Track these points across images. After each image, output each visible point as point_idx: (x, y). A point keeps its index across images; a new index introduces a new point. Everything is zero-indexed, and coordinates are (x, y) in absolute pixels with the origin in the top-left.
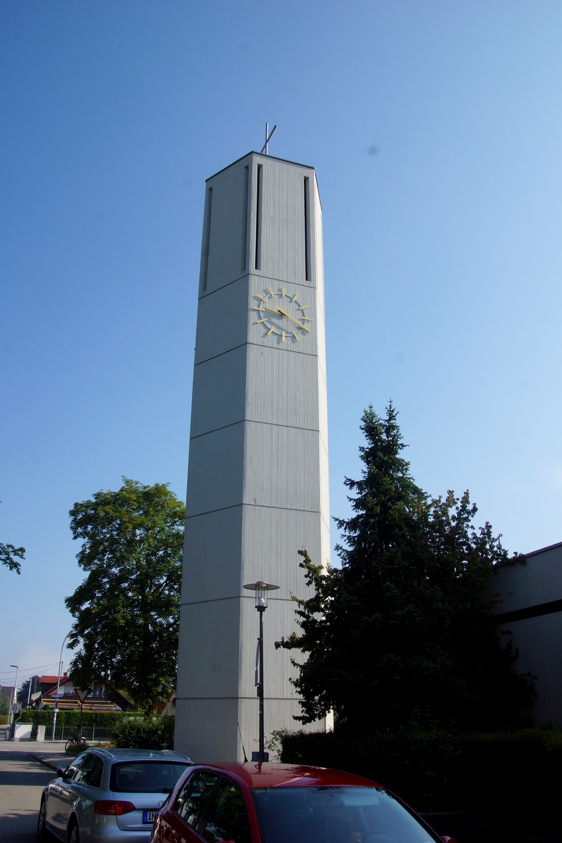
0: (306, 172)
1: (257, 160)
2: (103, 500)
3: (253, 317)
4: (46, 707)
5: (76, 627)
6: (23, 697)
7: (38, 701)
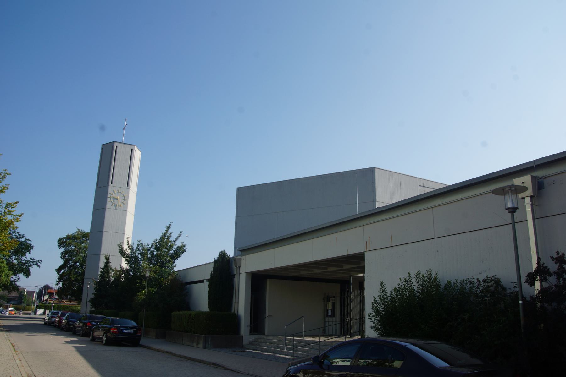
0: (132, 147)
1: (116, 144)
2: (68, 237)
3: (108, 200)
4: (50, 303)
5: (59, 278)
6: (40, 296)
7: (47, 300)
